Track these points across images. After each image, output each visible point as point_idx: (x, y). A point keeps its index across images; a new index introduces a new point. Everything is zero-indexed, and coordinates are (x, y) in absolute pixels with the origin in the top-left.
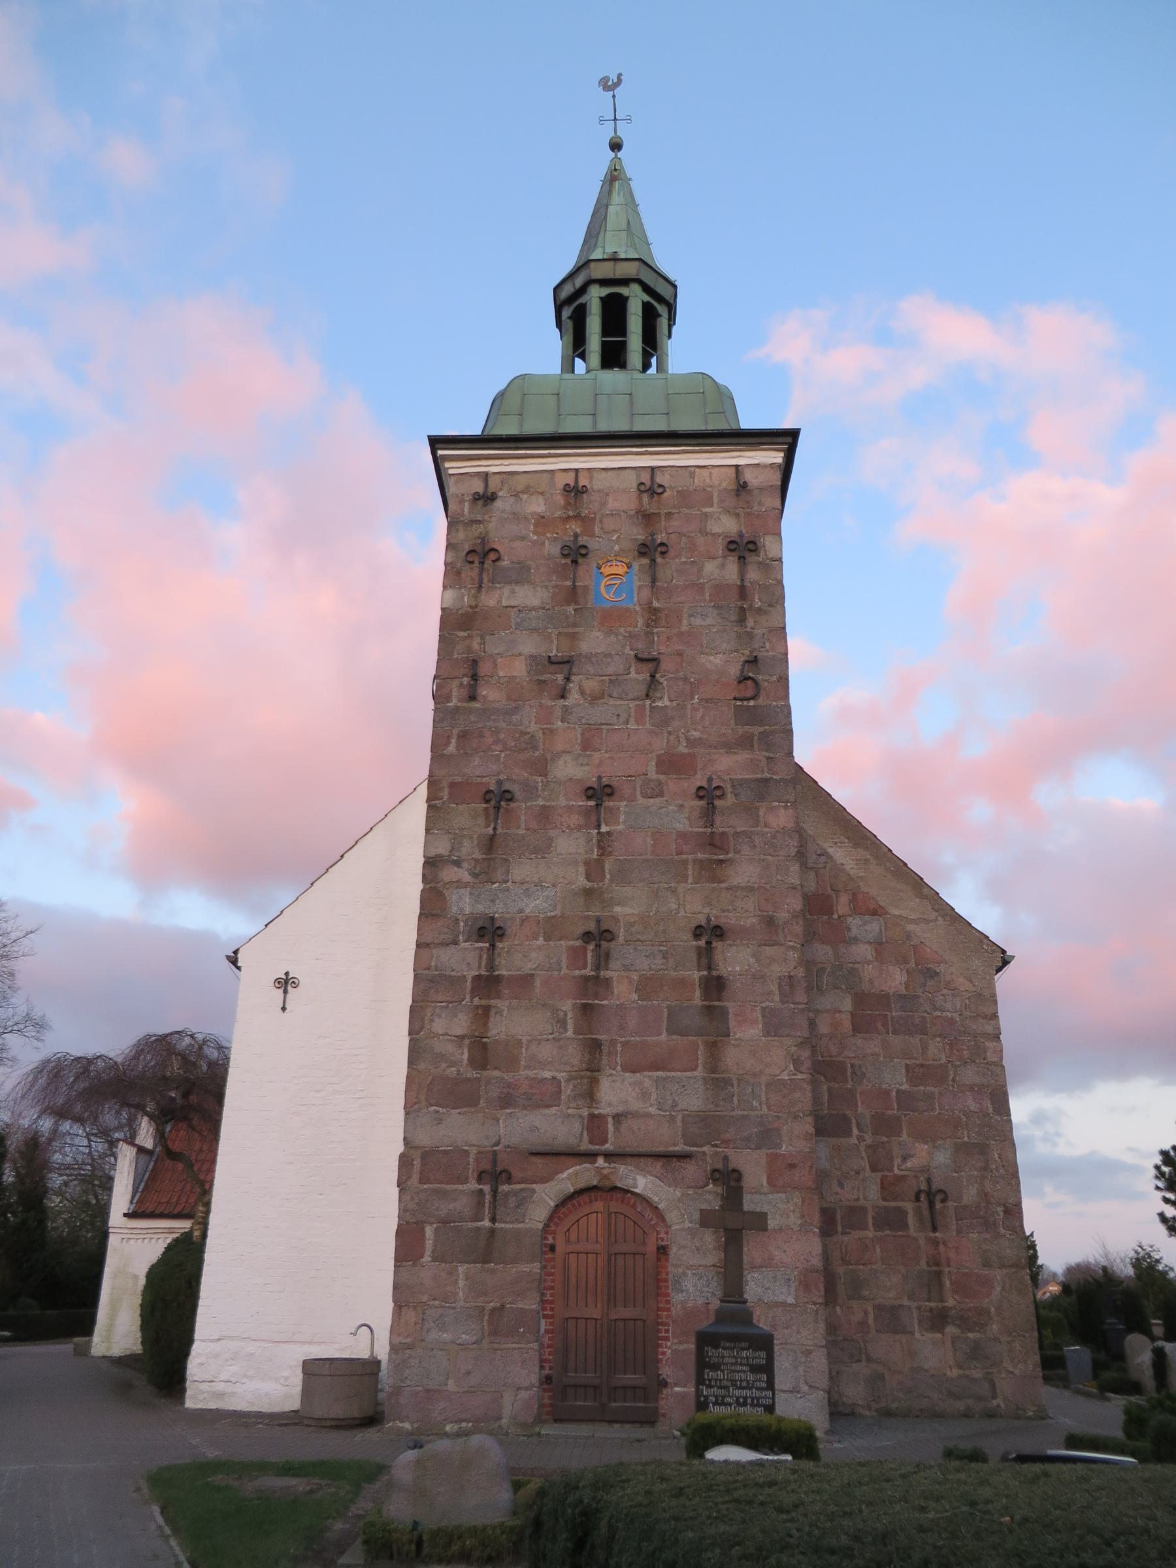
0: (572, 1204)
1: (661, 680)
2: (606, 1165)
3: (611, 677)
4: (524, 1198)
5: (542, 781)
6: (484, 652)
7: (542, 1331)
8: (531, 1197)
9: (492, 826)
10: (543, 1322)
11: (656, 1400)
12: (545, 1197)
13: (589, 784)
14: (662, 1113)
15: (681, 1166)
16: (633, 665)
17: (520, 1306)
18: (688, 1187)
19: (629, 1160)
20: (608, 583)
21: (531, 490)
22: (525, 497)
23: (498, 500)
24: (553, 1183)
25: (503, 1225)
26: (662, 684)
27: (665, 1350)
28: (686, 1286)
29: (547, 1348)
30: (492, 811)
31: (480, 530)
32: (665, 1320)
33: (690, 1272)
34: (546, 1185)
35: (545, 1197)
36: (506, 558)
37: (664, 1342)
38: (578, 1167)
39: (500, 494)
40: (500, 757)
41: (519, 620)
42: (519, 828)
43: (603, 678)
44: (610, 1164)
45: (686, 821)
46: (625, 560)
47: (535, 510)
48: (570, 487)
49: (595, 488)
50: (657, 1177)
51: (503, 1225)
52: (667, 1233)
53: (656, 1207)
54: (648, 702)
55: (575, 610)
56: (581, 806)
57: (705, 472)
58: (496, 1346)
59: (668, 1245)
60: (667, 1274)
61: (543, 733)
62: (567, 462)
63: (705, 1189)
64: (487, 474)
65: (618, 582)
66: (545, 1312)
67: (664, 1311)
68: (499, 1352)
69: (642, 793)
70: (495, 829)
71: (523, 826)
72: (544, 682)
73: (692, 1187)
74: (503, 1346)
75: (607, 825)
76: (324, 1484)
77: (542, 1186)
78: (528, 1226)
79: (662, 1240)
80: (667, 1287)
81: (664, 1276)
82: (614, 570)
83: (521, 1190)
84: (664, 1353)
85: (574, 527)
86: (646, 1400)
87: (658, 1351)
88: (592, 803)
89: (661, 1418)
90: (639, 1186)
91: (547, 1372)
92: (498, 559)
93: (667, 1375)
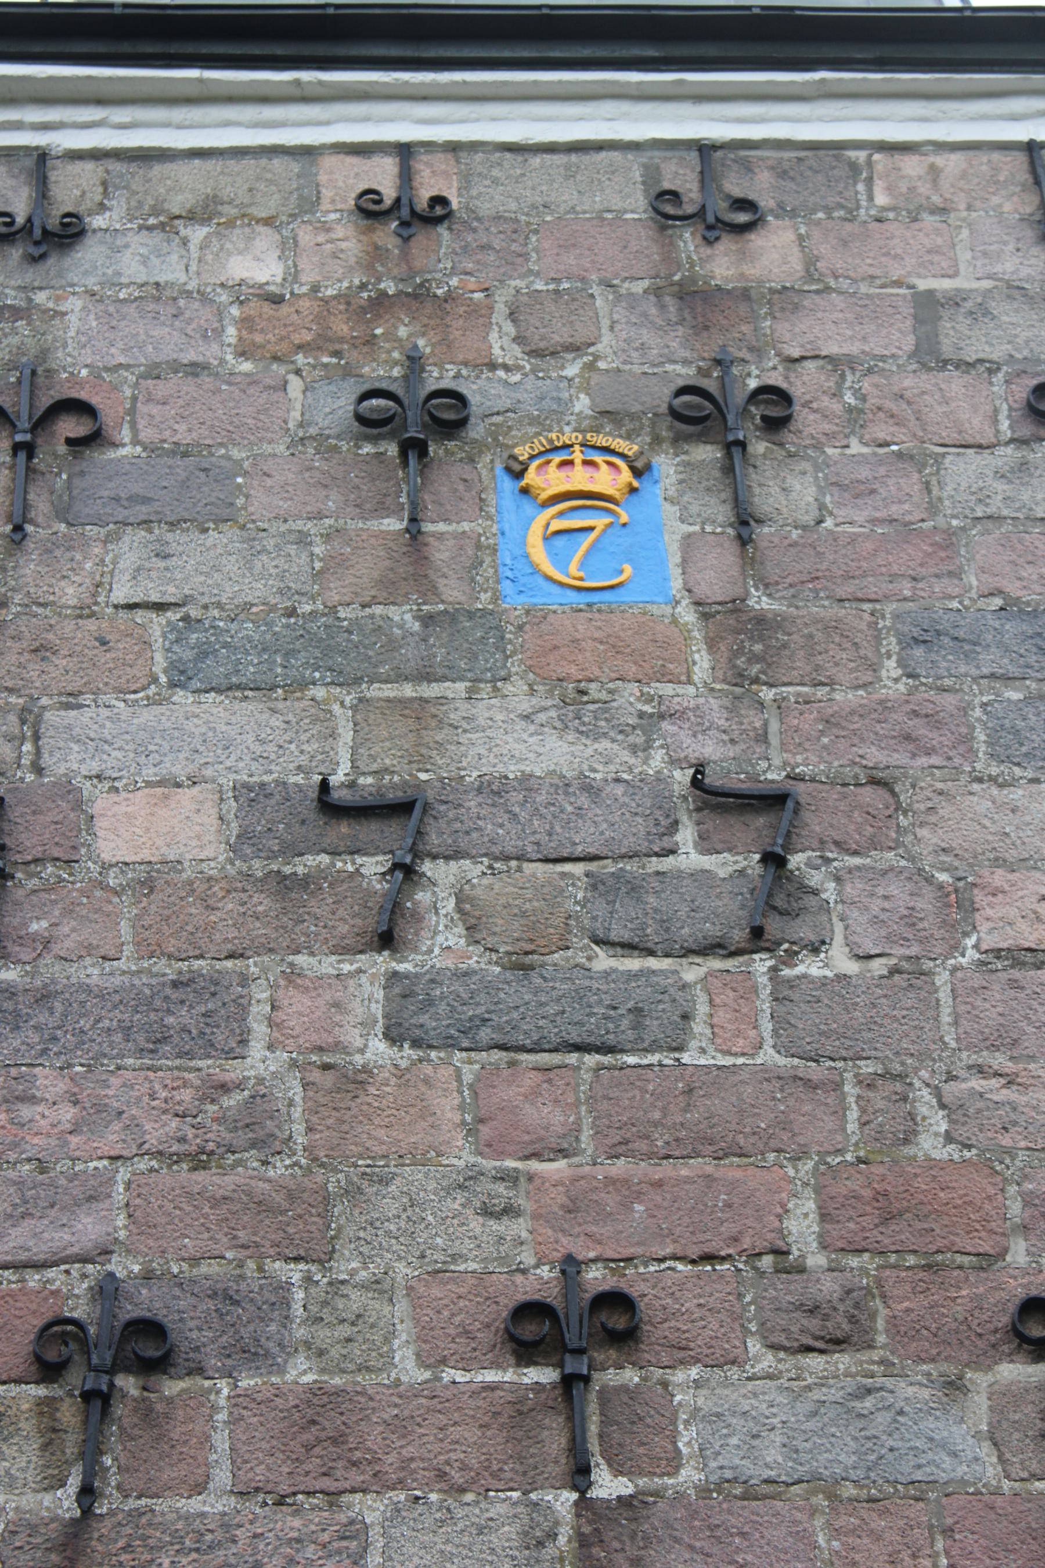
1: (815, 878)
3: (593, 866)
5: (308, 1280)
6: (38, 769)
9: (74, 1483)
13: (526, 1289)
16: (684, 818)
20: (557, 525)
21: (226, 209)
22: (198, 234)
23: (90, 241)
26: (815, 892)
30: (69, 1414)
31: (15, 340)
36: (126, 434)
39: (98, 221)
40: (111, 1181)
41: (188, 655)
42: (199, 1488)
43: (568, 867)
45: (985, 1450)
46: (620, 444)
47: (245, 275)
48: (380, 202)
49: (485, 208)
54: (761, 964)
55: (428, 620)
56: (492, 1387)
57: (912, 166)
61: (306, 1085)
62: (366, 119)
64: (42, 156)
65: (600, 521)
69: (669, 1475)
70: (87, 1493)
71: (222, 1477)
72: (304, 882)
75: (618, 1473)
76: (887, 1311)
82: (579, 479)
85: (403, 332)
88: (542, 1375)
92: (95, 439)
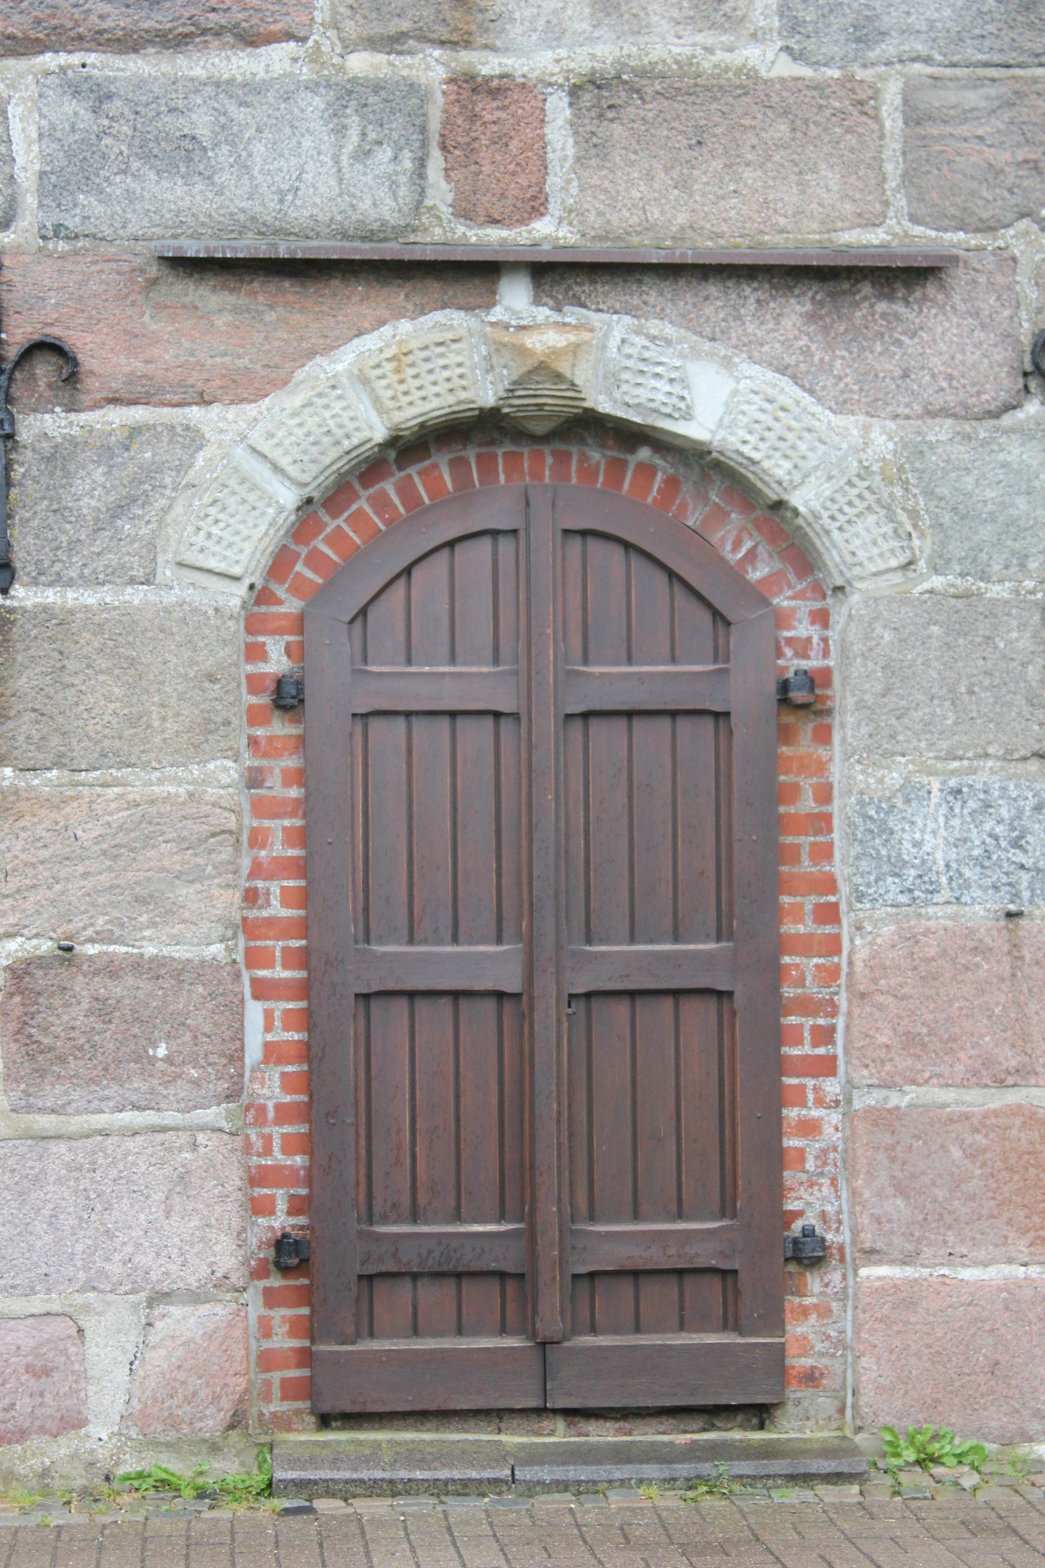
0: (373, 501)
2: (543, 313)
4: (152, 472)
7: (253, 1052)
8: (181, 468)
10: (255, 1011)
11: (775, 1321)
12: (150, 1117)
14: (806, 72)
15: (897, 316)
17: (150, 950)
18: (930, 413)
19: (653, 294)
24: (292, 400)
25: (50, 596)
27: (815, 1113)
28: (917, 844)
29: (279, 1121)
32: (813, 989)
33: (936, 785)
34: (251, 410)
35: (150, 1117)
37: (810, 1082)
38: (405, 326)
44: (559, 310)
50: (782, 370)
51: (50, 596)
52: (822, 618)
53: (779, 505)
58: (46, 1122)
59: (827, 672)
60: (825, 794)
63: (1007, 420)
66: (262, 973)
67: (808, 953)
68: (60, 1148)
73: (945, 412)
74: (76, 1123)
77: (232, 412)
78: (169, 598)
79: (802, 647)
80: (824, 852)
81: (807, 804)
83: (135, 431)
84: (810, 1128)
86: (730, 1322)
87: (779, 1120)
89: (794, 1392)
90: (698, 411)
91: (281, 1221)
93: (823, 1216)
